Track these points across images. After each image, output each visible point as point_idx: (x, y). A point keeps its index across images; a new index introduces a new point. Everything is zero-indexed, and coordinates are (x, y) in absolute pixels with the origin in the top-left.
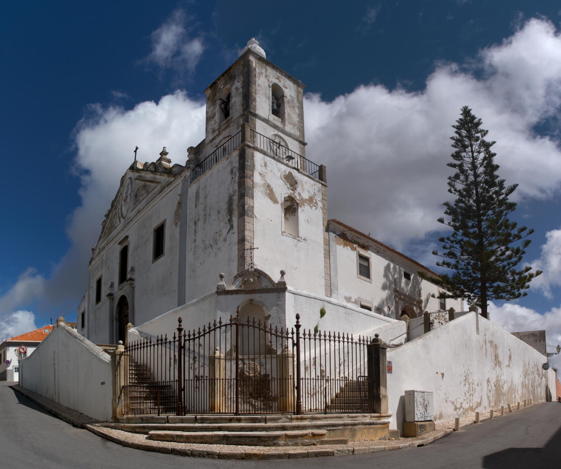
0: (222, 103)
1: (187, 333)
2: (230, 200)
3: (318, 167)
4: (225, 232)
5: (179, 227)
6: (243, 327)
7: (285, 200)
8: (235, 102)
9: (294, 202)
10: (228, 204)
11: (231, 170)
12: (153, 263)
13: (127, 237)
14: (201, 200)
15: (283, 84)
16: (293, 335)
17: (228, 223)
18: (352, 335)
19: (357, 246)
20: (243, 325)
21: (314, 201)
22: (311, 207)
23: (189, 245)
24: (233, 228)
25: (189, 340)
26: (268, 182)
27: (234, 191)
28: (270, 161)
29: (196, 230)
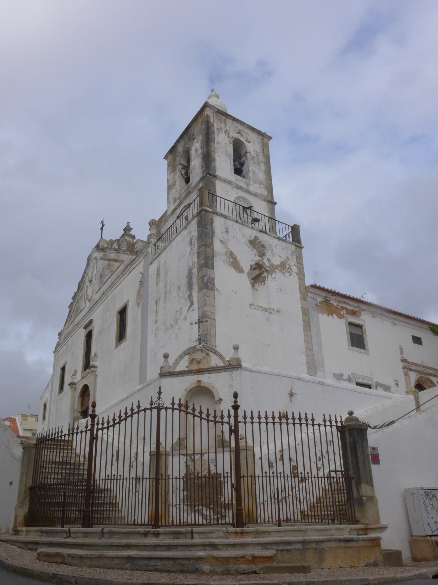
0: (182, 168)
1: (100, 421)
2: (189, 274)
3: (290, 228)
4: (186, 308)
5: (141, 308)
6: (166, 411)
7: (253, 268)
8: (194, 165)
9: (263, 269)
10: (188, 278)
11: (190, 240)
12: (116, 348)
13: (91, 322)
14: (162, 276)
15: (245, 139)
16: (229, 419)
17: (188, 299)
18: (341, 417)
19: (345, 312)
20: (166, 409)
21: (288, 266)
22: (284, 274)
23: (151, 327)
24: (193, 305)
25: (102, 429)
26: (231, 249)
27: (193, 263)
28: (232, 226)
29: (157, 310)
